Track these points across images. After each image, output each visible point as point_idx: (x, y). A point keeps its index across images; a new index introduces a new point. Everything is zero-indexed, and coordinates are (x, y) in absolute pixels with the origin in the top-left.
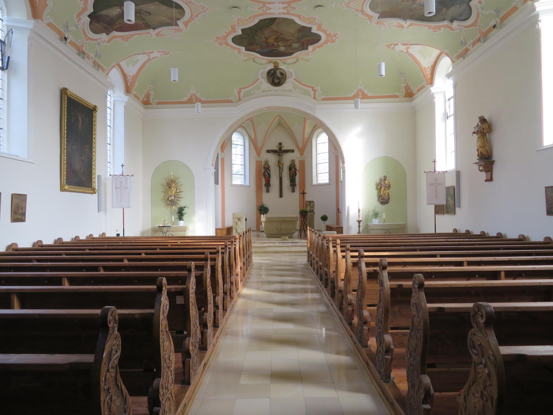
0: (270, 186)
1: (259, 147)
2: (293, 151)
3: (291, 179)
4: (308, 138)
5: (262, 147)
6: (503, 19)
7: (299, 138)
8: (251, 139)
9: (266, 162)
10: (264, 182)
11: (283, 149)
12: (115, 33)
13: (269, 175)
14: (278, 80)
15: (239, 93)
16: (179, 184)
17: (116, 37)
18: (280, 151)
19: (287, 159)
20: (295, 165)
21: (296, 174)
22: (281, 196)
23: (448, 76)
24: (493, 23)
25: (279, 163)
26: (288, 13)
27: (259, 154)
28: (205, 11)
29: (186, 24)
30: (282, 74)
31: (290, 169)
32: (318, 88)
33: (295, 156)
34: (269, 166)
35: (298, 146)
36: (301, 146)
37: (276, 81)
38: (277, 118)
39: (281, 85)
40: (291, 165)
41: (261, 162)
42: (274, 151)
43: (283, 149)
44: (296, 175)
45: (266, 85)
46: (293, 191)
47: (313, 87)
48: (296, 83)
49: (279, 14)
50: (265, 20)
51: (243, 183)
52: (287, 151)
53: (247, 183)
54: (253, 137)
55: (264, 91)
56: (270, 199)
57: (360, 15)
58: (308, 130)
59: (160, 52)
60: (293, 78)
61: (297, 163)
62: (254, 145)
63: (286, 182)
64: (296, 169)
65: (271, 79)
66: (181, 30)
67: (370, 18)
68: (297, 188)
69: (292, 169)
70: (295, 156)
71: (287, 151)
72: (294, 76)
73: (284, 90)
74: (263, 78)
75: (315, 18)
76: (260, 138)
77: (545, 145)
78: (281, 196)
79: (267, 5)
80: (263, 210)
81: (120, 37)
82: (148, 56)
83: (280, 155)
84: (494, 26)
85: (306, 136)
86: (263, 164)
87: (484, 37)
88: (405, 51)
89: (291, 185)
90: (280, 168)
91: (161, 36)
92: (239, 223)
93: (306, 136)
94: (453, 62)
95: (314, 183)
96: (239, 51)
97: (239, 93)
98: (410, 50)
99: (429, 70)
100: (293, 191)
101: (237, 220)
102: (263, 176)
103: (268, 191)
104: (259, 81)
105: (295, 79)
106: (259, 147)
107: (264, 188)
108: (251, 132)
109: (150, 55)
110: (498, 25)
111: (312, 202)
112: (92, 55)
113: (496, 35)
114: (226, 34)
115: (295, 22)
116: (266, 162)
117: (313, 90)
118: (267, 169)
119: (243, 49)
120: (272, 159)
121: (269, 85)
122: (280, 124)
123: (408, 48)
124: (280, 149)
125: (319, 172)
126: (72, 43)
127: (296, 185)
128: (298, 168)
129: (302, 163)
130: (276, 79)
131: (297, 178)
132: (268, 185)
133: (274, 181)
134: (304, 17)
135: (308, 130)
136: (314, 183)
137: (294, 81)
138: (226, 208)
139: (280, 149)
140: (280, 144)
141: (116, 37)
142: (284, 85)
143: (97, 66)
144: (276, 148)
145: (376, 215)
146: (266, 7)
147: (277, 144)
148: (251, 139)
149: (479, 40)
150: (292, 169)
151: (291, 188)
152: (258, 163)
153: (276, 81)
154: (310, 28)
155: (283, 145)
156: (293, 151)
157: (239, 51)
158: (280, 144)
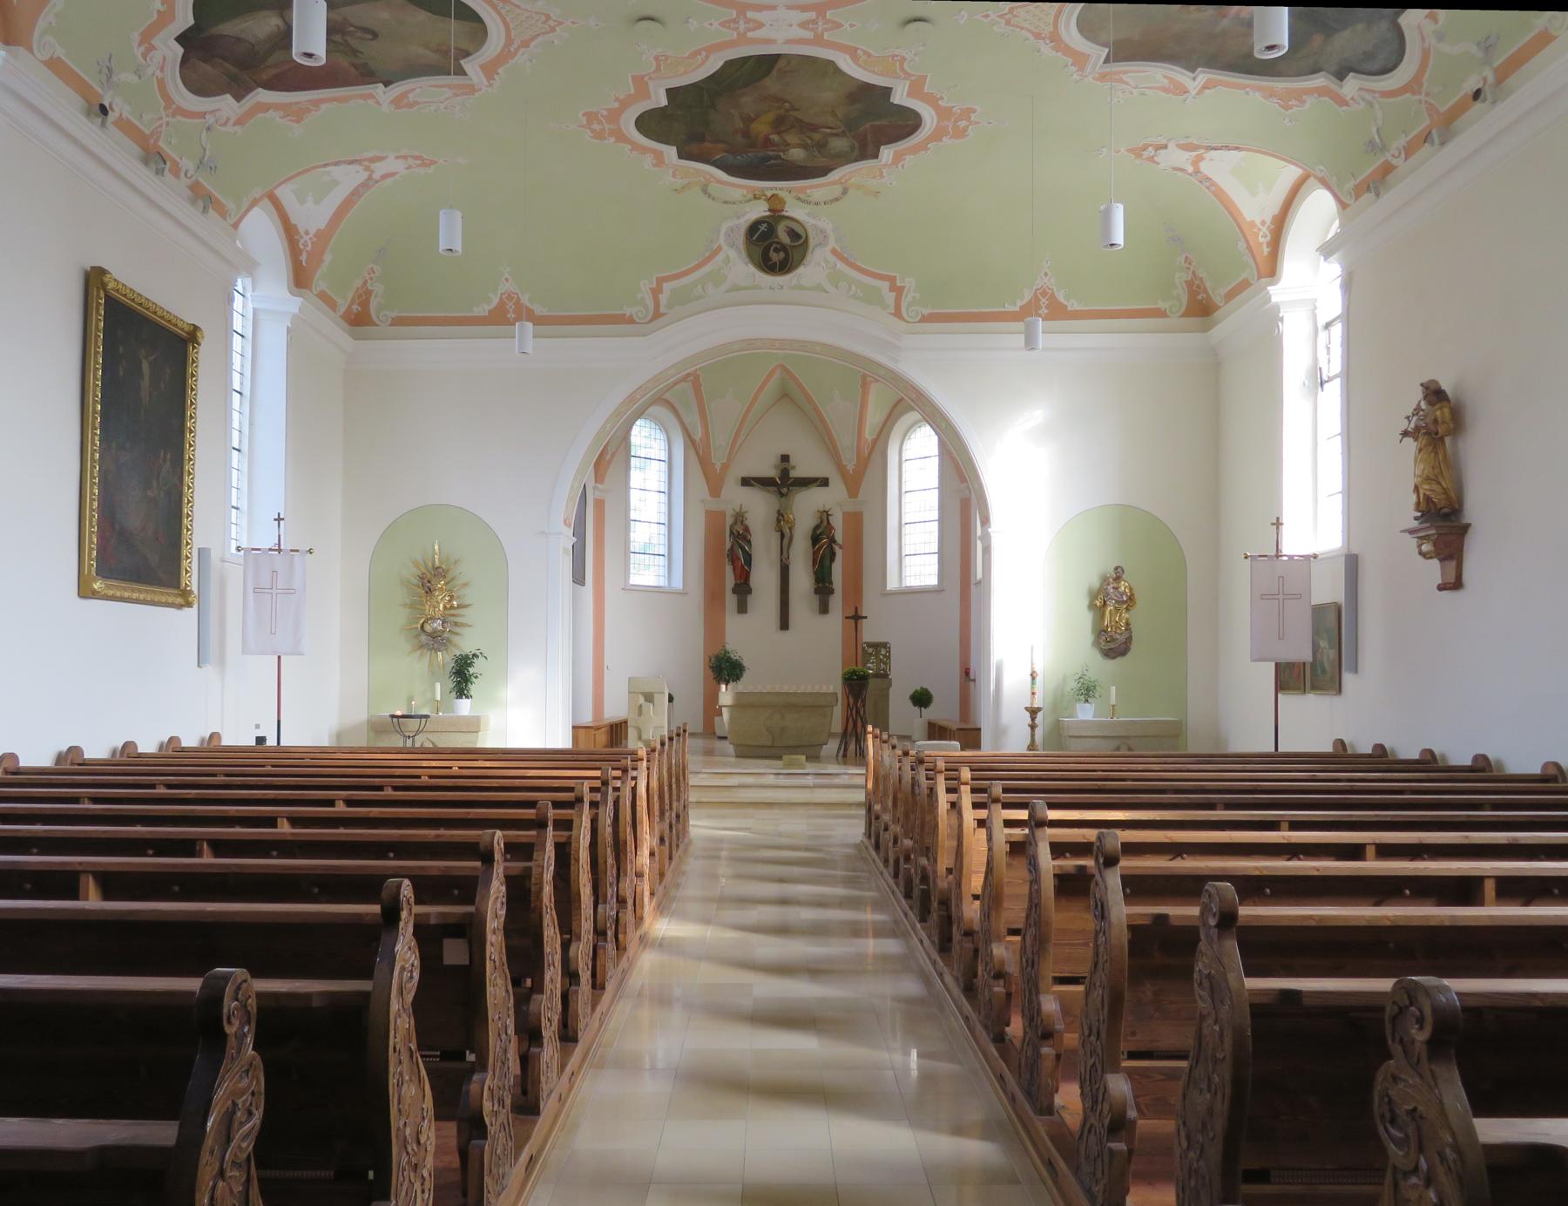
0: (749, 591)
1: (718, 466)
2: (824, 482)
3: (815, 573)
4: (875, 442)
5: (725, 467)
6: (1503, 74)
7: (845, 442)
8: (693, 442)
9: (740, 517)
10: (730, 580)
12: (262, 95)
13: (748, 558)
14: (782, 255)
15: (656, 292)
17: (266, 107)
18: (783, 482)
19: (806, 507)
20: (829, 527)
21: (833, 555)
22: (784, 624)
23: (1327, 250)
24: (1471, 84)
25: (778, 521)
26: (818, 41)
27: (715, 491)
28: (553, 30)
29: (490, 70)
30: (794, 235)
31: (815, 539)
32: (909, 283)
33: (832, 498)
34: (747, 529)
35: (841, 468)
36: (850, 467)
37: (776, 257)
38: (776, 376)
39: (789, 271)
40: (817, 527)
41: (723, 514)
42: (764, 482)
43: (794, 474)
45: (743, 270)
46: (824, 609)
47: (892, 280)
48: (840, 265)
49: (788, 42)
50: (745, 60)
51: (662, 582)
52: (806, 483)
53: (678, 584)
54: (698, 434)
55: (736, 288)
56: (749, 634)
57: (1047, 50)
58: (874, 417)
59: (405, 158)
60: (828, 249)
61: (837, 522)
62: (702, 462)
63: (802, 579)
64: (832, 540)
65: (758, 251)
66: (472, 89)
67: (1080, 60)
68: (836, 602)
69: (821, 536)
70: (832, 498)
71: (806, 483)
72: (832, 243)
73: (800, 287)
74: (732, 245)
75: (904, 59)
76: (720, 442)
78: (784, 624)
79: (750, 14)
80: (725, 668)
81: (277, 107)
82: (367, 169)
83: (782, 495)
84: (1477, 95)
85: (869, 435)
86: (729, 521)
87: (1445, 126)
88: (1190, 169)
89: (817, 591)
90: (782, 536)
91: (411, 105)
93: (869, 435)
94: (1343, 205)
95: (892, 584)
96: (659, 159)
97: (656, 292)
98: (1205, 167)
99: (1264, 229)
100: (824, 609)
102: (728, 560)
103: (742, 608)
104: (720, 257)
105: (834, 252)
106: (718, 466)
108: (693, 419)
109: (373, 166)
110: (1487, 91)
111: (885, 645)
112: (188, 164)
113: (1481, 124)
114: (616, 105)
115: (838, 71)
116: (740, 517)
117: (893, 288)
118: (741, 537)
119: (671, 152)
120: (758, 508)
121: (752, 268)
122: (784, 396)
123: (1200, 158)
124: (785, 473)
125: (907, 550)
126: (125, 126)
127: (832, 591)
128: (839, 537)
129: (855, 521)
130: (776, 250)
131: (837, 569)
132: (743, 589)
133: (764, 577)
134: (869, 55)
135: (874, 417)
136: (892, 584)
137: (832, 259)
139: (785, 473)
140: (785, 458)
141: (266, 107)
142: (801, 270)
143: (202, 198)
144: (771, 472)
146: (748, 21)
147: (773, 459)
148: (693, 442)
149: (1427, 138)
150: (821, 536)
151: (815, 600)
152: (714, 519)
153: (776, 257)
154: (887, 91)
155: (793, 461)
156: (824, 482)
157: (659, 159)
158: (785, 458)
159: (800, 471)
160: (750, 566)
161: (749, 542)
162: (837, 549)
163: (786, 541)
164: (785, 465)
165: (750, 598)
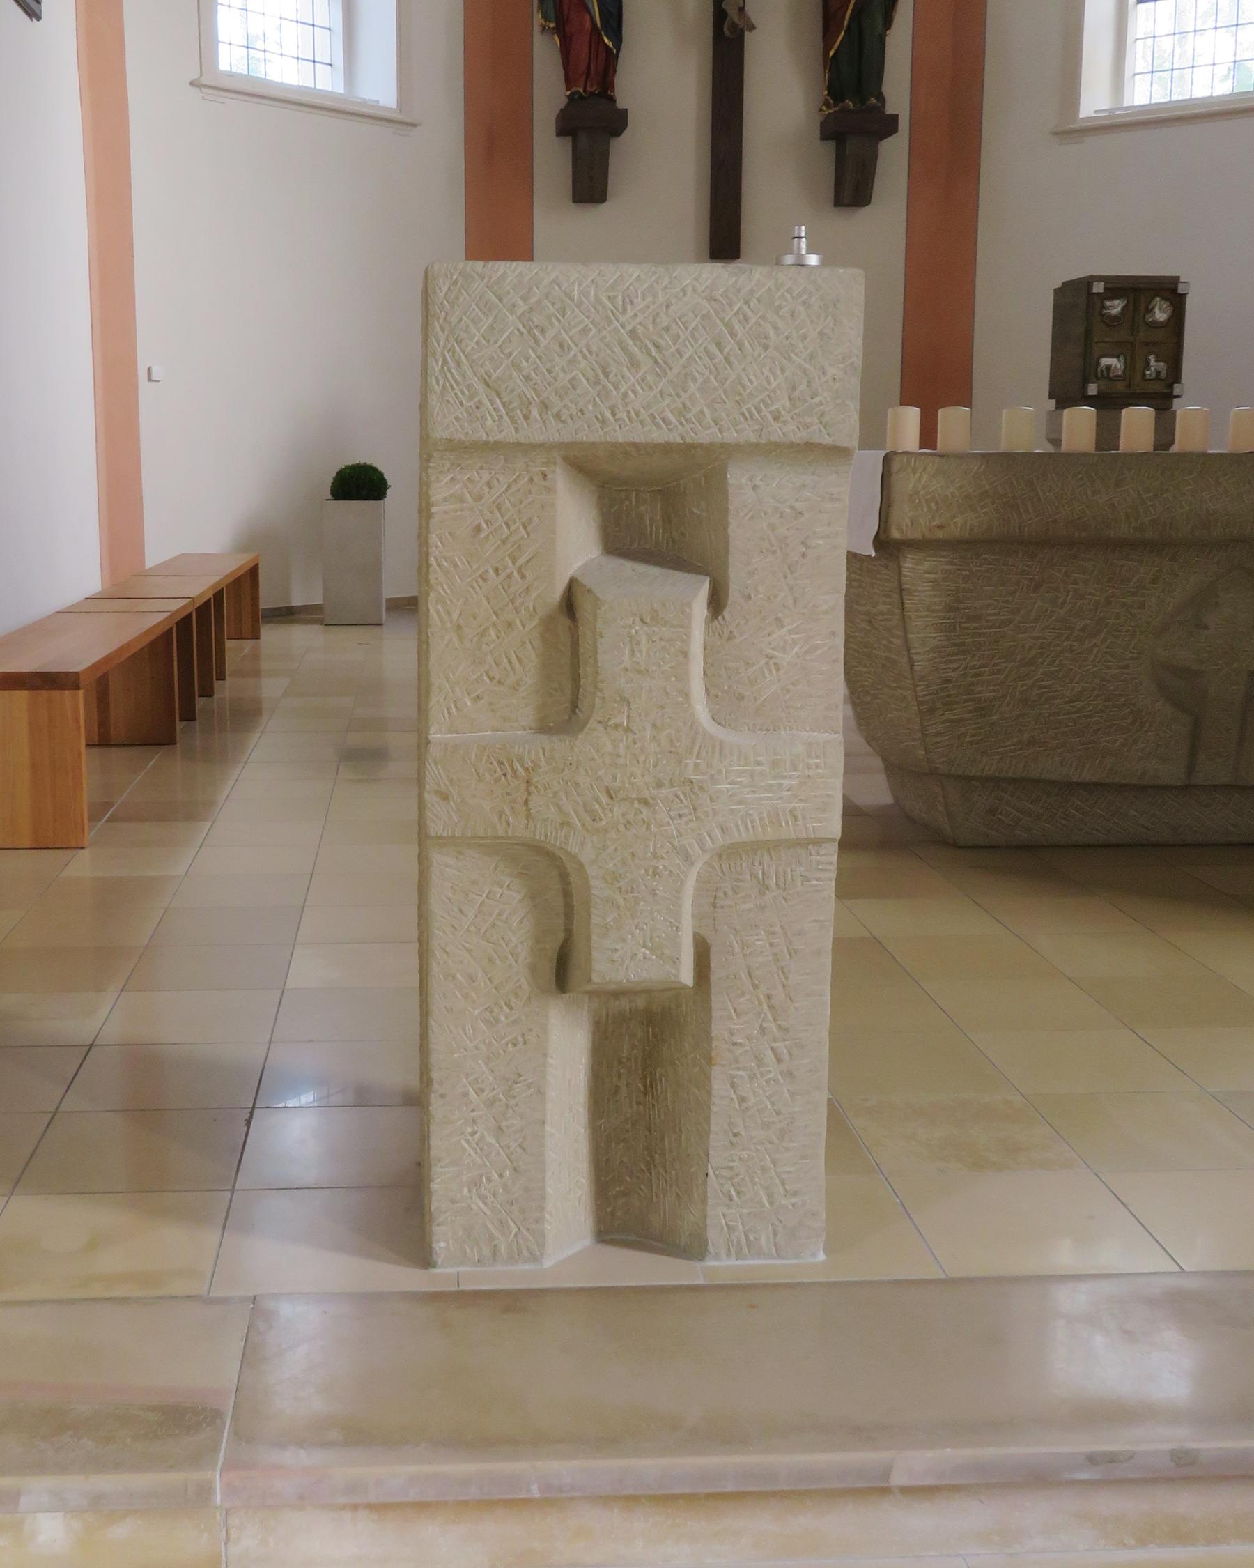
0: (617, 122)
10: (548, 90)
16: (225, 690)
44: (888, 23)
46: (852, 188)
51: (328, 82)
53: (379, 87)
63: (783, 91)
68: (894, 156)
77: (1082, 115)
78: (724, 242)
92: (650, 617)
95: (1094, 100)
100: (852, 188)
101: (574, 537)
103: (590, 186)
107: (551, 158)
111: (1171, 291)
132: (594, 122)
136: (1094, 100)
138: (151, 348)
145: (546, 407)
151: (825, 155)
160: (618, 37)
165: (620, 148)
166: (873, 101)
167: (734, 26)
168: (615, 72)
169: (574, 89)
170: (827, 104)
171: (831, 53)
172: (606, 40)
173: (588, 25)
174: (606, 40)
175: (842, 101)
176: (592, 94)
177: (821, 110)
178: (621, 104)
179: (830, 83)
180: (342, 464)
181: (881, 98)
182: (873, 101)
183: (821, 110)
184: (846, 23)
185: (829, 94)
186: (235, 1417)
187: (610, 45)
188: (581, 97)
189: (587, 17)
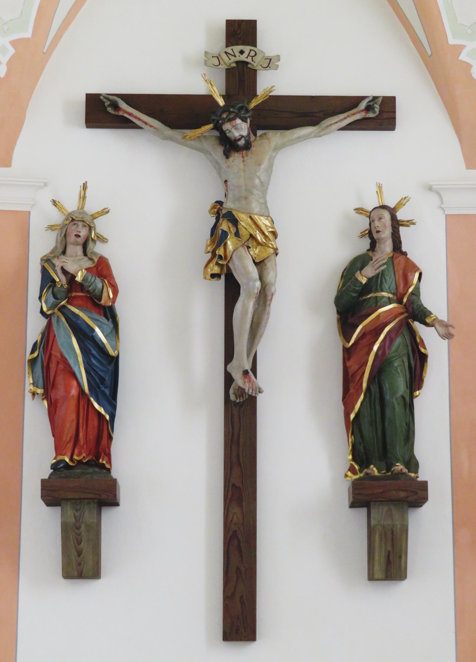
0: (107, 496)
3: (354, 427)
11: (270, 83)
34: (102, 269)
41: (22, 219)
42: (176, 114)
43: (270, 83)
44: (416, 380)
46: (387, 560)
63: (304, 454)
100: (387, 560)
103: (81, 559)
124: (241, 78)
127: (417, 495)
128: (434, 296)
140: (241, 32)
151: (355, 524)
155: (267, 42)
158: (241, 32)
159: (288, 75)
160: (111, 400)
161: (110, 314)
162: (428, 335)
163: (245, 306)
164: (240, 52)
166: (399, 467)
167: (240, 392)
168: (110, 438)
169: (60, 458)
170: (352, 469)
171: (352, 416)
172: (96, 405)
173: (74, 392)
174: (96, 405)
175: (368, 467)
176: (80, 462)
177: (346, 476)
178: (115, 474)
179: (354, 446)
180: (333, 302)
181: (412, 464)
182: (399, 467)
183: (346, 476)
184: (365, 385)
185: (354, 459)
186: (25, 362)
187: (102, 411)
188: (67, 466)
189: (75, 383)
